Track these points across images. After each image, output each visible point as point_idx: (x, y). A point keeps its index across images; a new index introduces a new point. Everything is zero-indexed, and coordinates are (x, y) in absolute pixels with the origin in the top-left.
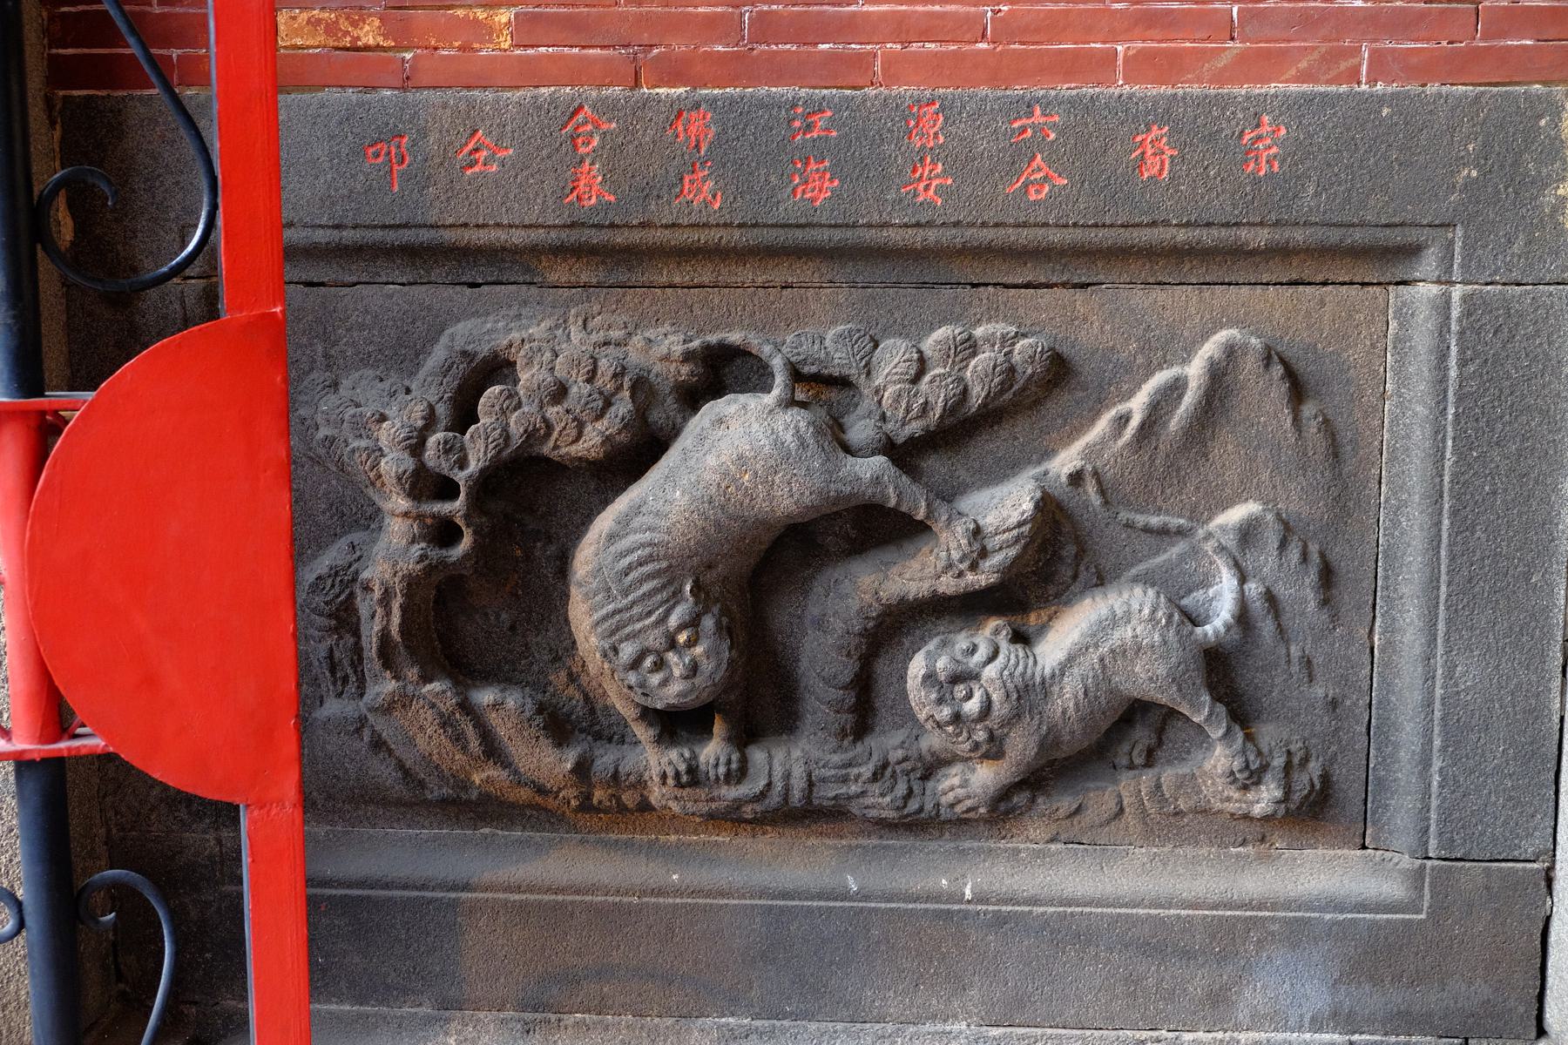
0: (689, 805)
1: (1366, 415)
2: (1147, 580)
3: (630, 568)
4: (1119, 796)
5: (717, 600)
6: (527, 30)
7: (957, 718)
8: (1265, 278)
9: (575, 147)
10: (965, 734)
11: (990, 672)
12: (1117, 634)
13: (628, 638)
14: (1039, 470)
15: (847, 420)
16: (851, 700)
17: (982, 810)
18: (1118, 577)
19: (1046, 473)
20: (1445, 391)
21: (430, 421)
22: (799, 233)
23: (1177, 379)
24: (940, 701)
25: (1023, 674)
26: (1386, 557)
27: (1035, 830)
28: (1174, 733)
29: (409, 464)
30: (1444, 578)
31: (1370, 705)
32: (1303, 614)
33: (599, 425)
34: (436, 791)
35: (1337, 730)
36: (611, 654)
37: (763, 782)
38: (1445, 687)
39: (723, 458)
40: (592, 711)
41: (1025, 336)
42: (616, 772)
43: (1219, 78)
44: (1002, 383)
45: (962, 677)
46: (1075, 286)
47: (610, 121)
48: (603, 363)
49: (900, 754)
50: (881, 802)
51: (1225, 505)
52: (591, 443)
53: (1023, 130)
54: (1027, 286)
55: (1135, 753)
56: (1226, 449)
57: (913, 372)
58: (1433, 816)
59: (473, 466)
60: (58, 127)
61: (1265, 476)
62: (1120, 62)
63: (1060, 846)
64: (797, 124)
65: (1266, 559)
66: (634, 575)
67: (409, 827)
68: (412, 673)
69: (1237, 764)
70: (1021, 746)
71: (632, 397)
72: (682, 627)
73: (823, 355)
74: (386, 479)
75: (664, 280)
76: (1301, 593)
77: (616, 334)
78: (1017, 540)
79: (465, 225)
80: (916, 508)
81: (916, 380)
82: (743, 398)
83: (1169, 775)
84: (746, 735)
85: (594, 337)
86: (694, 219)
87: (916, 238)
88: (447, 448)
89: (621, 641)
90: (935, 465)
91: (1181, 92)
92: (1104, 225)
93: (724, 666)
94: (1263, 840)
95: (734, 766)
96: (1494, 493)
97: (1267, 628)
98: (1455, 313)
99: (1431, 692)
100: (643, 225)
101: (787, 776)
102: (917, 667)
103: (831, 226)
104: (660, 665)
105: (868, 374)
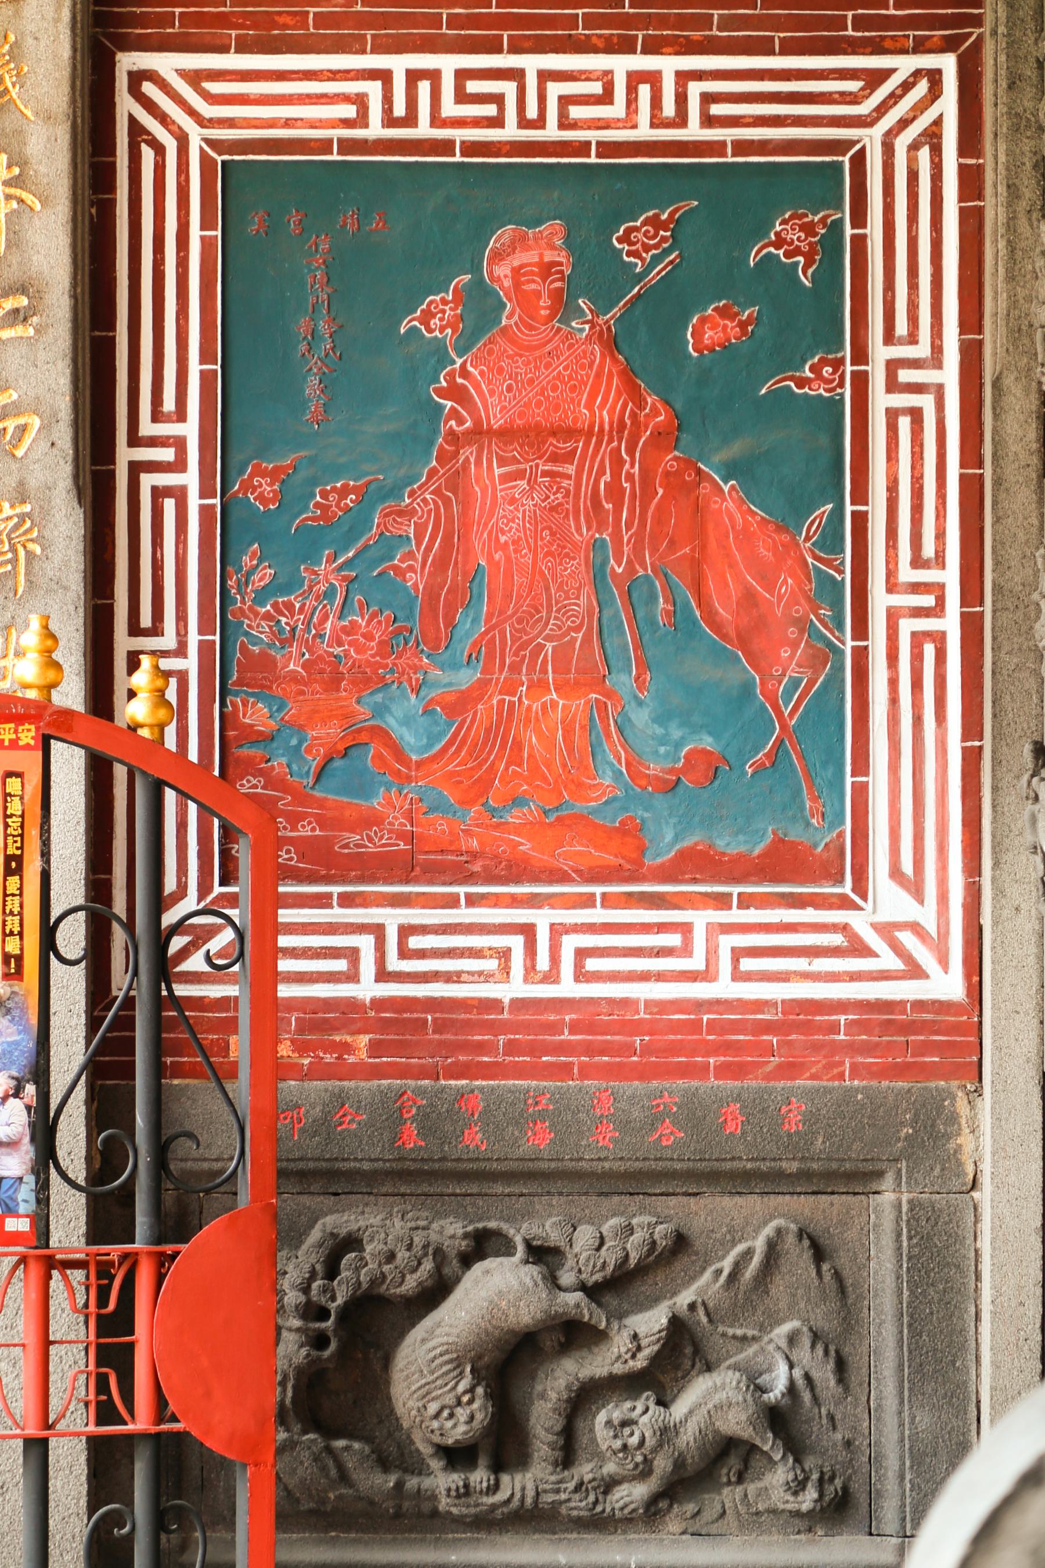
0: (463, 1509)
1: (860, 1269)
2: (736, 1367)
3: (435, 1358)
4: (723, 1502)
5: (483, 1379)
6: (375, 1049)
7: (625, 1447)
8: (799, 1190)
9: (402, 1114)
10: (630, 1458)
11: (645, 1419)
12: (717, 1396)
13: (433, 1399)
14: (671, 1302)
15: (559, 1273)
16: (561, 1442)
17: (641, 1511)
18: (719, 1366)
19: (675, 1304)
20: (901, 1254)
21: (313, 1275)
22: (531, 1164)
23: (749, 1248)
24: (615, 1437)
25: (663, 1421)
26: (875, 1353)
27: (673, 1525)
28: (757, 1461)
29: (302, 1298)
30: (906, 1364)
31: (870, 1444)
32: (827, 1388)
33: (415, 1276)
34: (306, 1505)
35: (851, 1460)
36: (422, 1410)
37: (509, 1493)
38: (910, 1429)
39: (490, 1293)
40: (402, 1455)
41: (661, 1223)
42: (419, 1489)
43: (768, 1077)
44: (648, 1250)
45: (625, 1423)
46: (690, 1195)
47: (422, 1099)
48: (416, 1240)
49: (591, 1476)
50: (579, 1506)
51: (779, 1322)
52: (411, 1284)
53: (658, 1106)
54: (662, 1194)
55: (731, 1474)
56: (779, 1287)
57: (597, 1244)
58: (908, 1509)
59: (340, 1301)
60: (96, 1102)
61: (802, 1305)
62: (712, 1068)
63: (688, 1537)
64: (530, 1101)
65: (804, 1354)
66: (437, 1362)
67: (284, 1532)
68: (297, 1428)
69: (791, 1476)
70: (662, 1464)
71: (434, 1258)
72: (465, 1392)
73: (544, 1235)
74: (287, 1309)
75: (450, 1191)
76: (825, 1375)
77: (422, 1223)
78: (658, 1340)
79: (336, 1159)
80: (600, 1322)
81: (598, 1249)
82: (499, 1259)
83: (752, 1488)
84: (498, 1467)
85: (410, 1225)
86: (471, 1155)
87: (598, 1167)
88: (324, 1290)
89: (429, 1402)
90: (612, 1300)
91: (746, 1086)
92: (705, 1160)
93: (489, 1416)
94: (810, 1530)
95: (492, 1482)
96: (932, 1313)
97: (806, 1396)
98: (904, 1209)
99: (903, 1434)
100: (440, 1160)
101: (523, 1489)
102: (602, 1417)
103: (549, 1160)
104: (451, 1415)
105: (571, 1246)
